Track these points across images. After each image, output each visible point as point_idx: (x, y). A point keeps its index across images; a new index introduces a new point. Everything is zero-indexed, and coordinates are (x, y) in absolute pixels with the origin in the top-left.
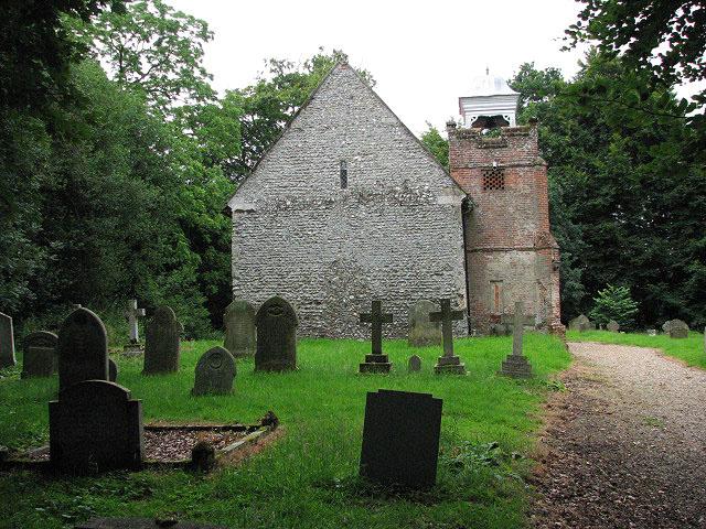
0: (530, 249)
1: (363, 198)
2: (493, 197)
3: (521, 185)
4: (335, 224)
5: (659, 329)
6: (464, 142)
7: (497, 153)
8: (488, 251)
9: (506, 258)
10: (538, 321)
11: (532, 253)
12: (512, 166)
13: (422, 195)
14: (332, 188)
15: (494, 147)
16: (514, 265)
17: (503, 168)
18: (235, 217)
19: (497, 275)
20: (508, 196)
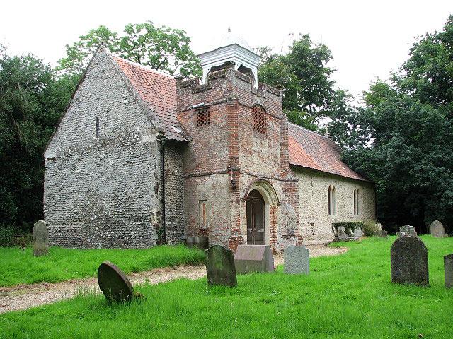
1: (105, 142)
3: (219, 119)
4: (89, 165)
5: (406, 67)
6: (185, 90)
7: (205, 95)
8: (200, 176)
9: (209, 181)
11: (226, 176)
12: (97, 125)
14: (91, 139)
15: (202, 91)
16: (214, 186)
17: (207, 107)
18: (46, 163)
19: (203, 195)
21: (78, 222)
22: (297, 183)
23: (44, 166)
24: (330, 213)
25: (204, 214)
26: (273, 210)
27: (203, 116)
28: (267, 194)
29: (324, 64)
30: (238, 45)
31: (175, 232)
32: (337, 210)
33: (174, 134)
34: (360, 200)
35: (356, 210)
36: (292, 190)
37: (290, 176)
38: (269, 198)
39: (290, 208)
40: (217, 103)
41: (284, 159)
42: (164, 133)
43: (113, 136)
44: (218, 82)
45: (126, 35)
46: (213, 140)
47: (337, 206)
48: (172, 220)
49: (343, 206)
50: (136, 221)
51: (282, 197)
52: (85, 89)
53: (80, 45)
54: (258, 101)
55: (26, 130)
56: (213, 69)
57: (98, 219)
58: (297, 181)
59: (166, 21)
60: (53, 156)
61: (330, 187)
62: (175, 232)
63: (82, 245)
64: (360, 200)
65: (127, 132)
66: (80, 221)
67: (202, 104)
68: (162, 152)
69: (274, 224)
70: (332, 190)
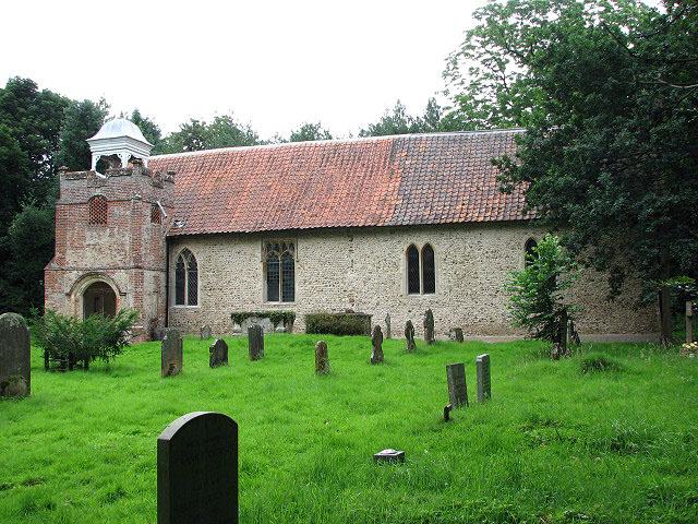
61: (412, 251)
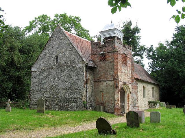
0: (111, 80)
1: (61, 66)
2: (102, 64)
3: (110, 59)
7: (104, 49)
8: (99, 81)
9: (105, 83)
10: (108, 112)
11: (113, 82)
12: (107, 53)
13: (74, 64)
16: (107, 86)
17: (105, 54)
18: (32, 73)
20: (106, 63)
21: (47, 98)
22: (137, 85)
23: (31, 74)
24: (143, 97)
25: (102, 97)
26: (128, 96)
27: (103, 57)
28: (126, 89)
29: (136, 35)
30: (117, 29)
31: (90, 104)
32: (146, 96)
33: (91, 64)
34: (154, 92)
35: (153, 96)
36: (135, 88)
37: (134, 82)
38: (127, 91)
39: (134, 95)
40: (109, 52)
41: (132, 76)
42: (87, 64)
43: (64, 64)
44: (110, 44)
45: (55, 18)
46: (107, 67)
47: (146, 94)
48: (89, 99)
49: (148, 94)
50: (75, 99)
51: (131, 91)
52: (51, 43)
53: (34, 21)
54: (124, 52)
55: (17, 57)
56: (106, 38)
57: (57, 97)
58: (137, 84)
59: (71, 13)
60: (36, 70)
62: (90, 104)
63: (48, 108)
64: (154, 92)
65: (71, 62)
66: (48, 98)
67: (103, 52)
68: (86, 71)
69: (129, 101)
70: (144, 87)
